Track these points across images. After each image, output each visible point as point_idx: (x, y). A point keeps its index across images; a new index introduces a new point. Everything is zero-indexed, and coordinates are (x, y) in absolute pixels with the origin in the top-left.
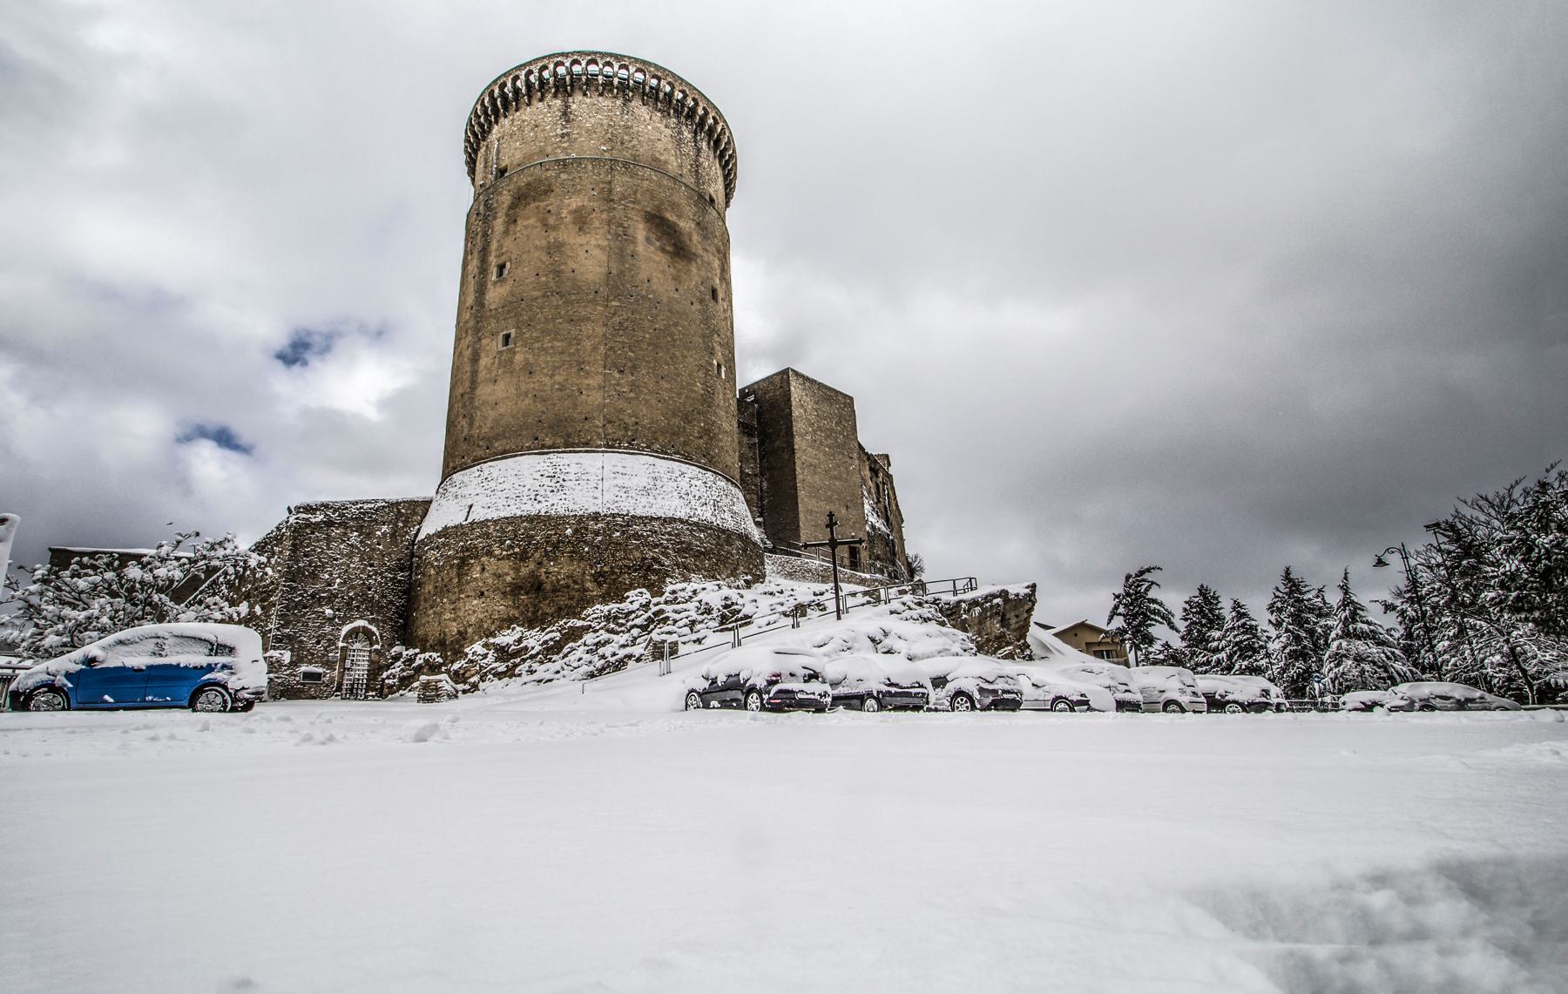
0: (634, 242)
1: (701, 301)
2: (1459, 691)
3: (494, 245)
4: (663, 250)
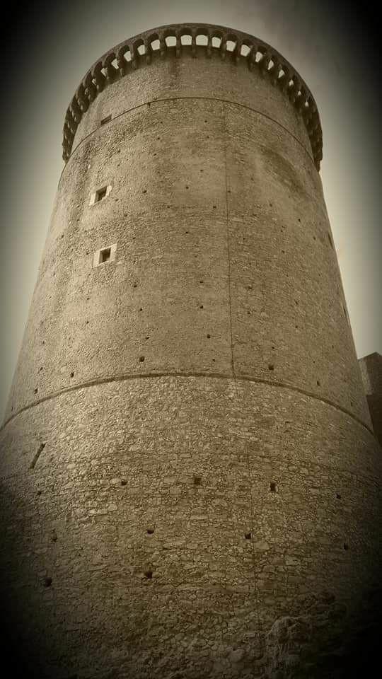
0: (252, 167)
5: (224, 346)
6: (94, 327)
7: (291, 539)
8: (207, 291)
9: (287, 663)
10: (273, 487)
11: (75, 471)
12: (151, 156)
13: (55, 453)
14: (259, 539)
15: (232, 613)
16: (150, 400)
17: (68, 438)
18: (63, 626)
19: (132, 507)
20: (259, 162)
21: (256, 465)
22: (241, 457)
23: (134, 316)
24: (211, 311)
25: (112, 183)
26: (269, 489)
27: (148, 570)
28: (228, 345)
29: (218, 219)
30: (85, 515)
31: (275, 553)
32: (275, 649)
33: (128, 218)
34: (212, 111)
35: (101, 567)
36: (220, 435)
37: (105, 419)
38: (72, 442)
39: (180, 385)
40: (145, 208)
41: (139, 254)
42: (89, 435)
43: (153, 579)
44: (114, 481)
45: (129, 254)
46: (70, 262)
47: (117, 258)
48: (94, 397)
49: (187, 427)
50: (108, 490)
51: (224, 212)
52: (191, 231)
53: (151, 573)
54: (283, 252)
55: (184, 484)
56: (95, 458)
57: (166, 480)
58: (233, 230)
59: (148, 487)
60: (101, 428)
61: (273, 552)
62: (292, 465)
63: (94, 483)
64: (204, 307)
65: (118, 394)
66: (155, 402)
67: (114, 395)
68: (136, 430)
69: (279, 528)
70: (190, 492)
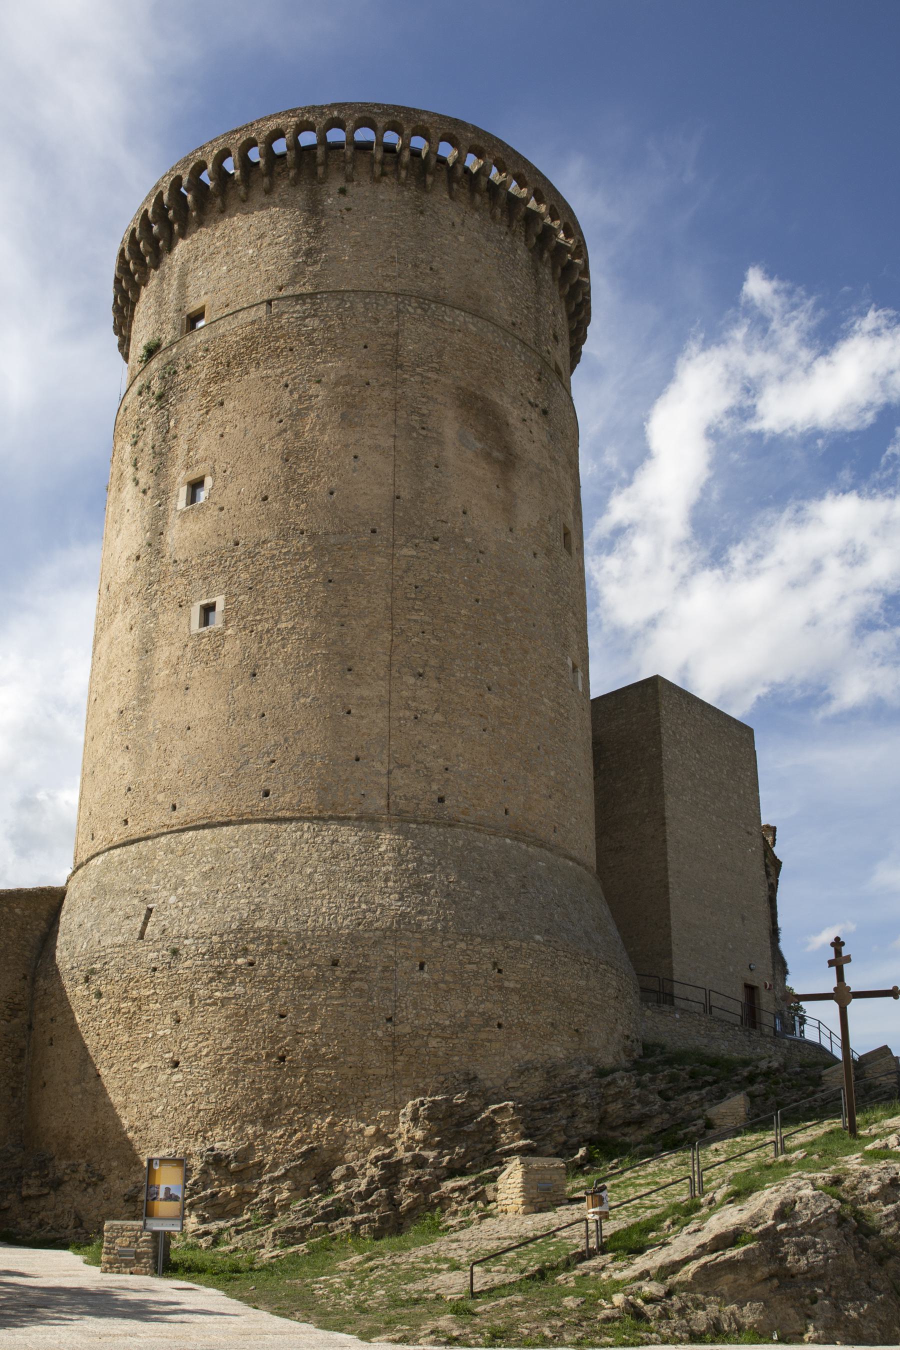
0: (440, 443)
1: (549, 552)
2: (580, 674)
3: (181, 447)
4: (488, 456)
5: (378, 773)
6: (199, 736)
7: (436, 1020)
8: (358, 685)
9: (417, 1138)
10: (422, 967)
11: (193, 947)
12: (274, 423)
13: (166, 923)
14: (402, 1022)
15: (367, 1094)
16: (279, 857)
17: (180, 904)
18: (196, 1105)
19: (261, 991)
20: (450, 425)
21: (405, 942)
22: (388, 933)
23: (253, 725)
24: (362, 717)
25: (213, 473)
26: (417, 968)
27: (280, 1054)
28: (385, 771)
29: (379, 553)
30: (210, 998)
31: (417, 1035)
32: (406, 1126)
33: (241, 549)
34: (377, 321)
35: (232, 1051)
36: (364, 906)
37: (224, 881)
38: (186, 910)
39: (317, 836)
40: (266, 533)
41: (258, 618)
42: (206, 904)
43: (286, 1063)
44: (240, 961)
45: (243, 618)
46: (155, 614)
47: (226, 622)
48: (207, 848)
49: (324, 896)
50: (234, 971)
51: (388, 540)
52: (336, 577)
53: (285, 1057)
54: (477, 601)
55: (319, 966)
56: (216, 934)
57: (300, 961)
58: (399, 573)
59: (279, 969)
60: (220, 895)
61: (415, 1035)
62: (448, 939)
63: (217, 963)
64: (352, 711)
65: (237, 847)
66: (285, 860)
67: (232, 848)
68: (263, 900)
69: (425, 1009)
70: (327, 974)
